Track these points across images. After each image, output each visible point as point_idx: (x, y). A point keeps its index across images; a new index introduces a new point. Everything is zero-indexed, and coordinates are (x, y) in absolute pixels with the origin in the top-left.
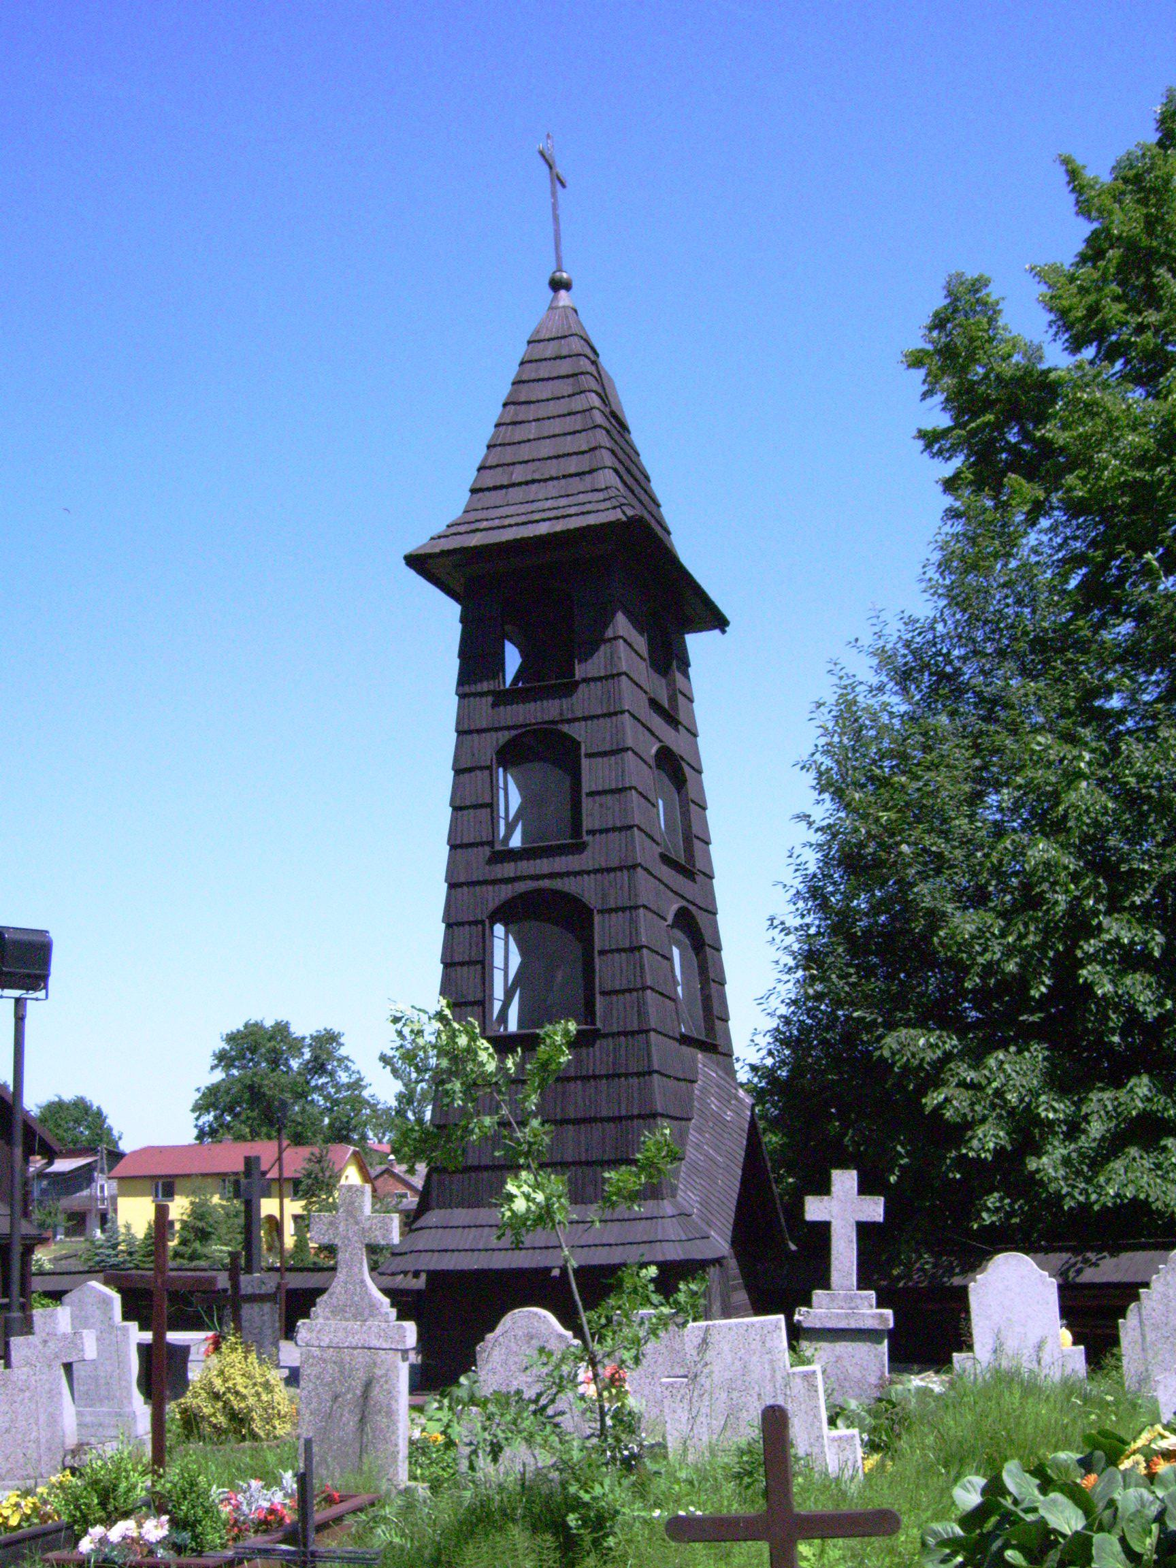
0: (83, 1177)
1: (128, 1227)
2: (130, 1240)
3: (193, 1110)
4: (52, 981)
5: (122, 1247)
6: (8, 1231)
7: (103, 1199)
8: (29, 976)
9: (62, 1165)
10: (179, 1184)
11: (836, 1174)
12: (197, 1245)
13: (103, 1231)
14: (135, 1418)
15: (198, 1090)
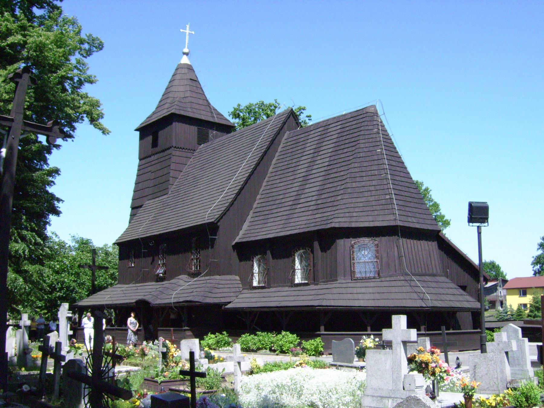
0: (493, 289)
1: (511, 306)
2: (512, 310)
3: (532, 265)
4: (490, 219)
5: (509, 313)
6: (480, 307)
7: (501, 296)
8: (481, 218)
9: (489, 284)
10: (528, 291)
11: (442, 327)
12: (536, 312)
13: (502, 307)
14: (528, 371)
15: (533, 257)
